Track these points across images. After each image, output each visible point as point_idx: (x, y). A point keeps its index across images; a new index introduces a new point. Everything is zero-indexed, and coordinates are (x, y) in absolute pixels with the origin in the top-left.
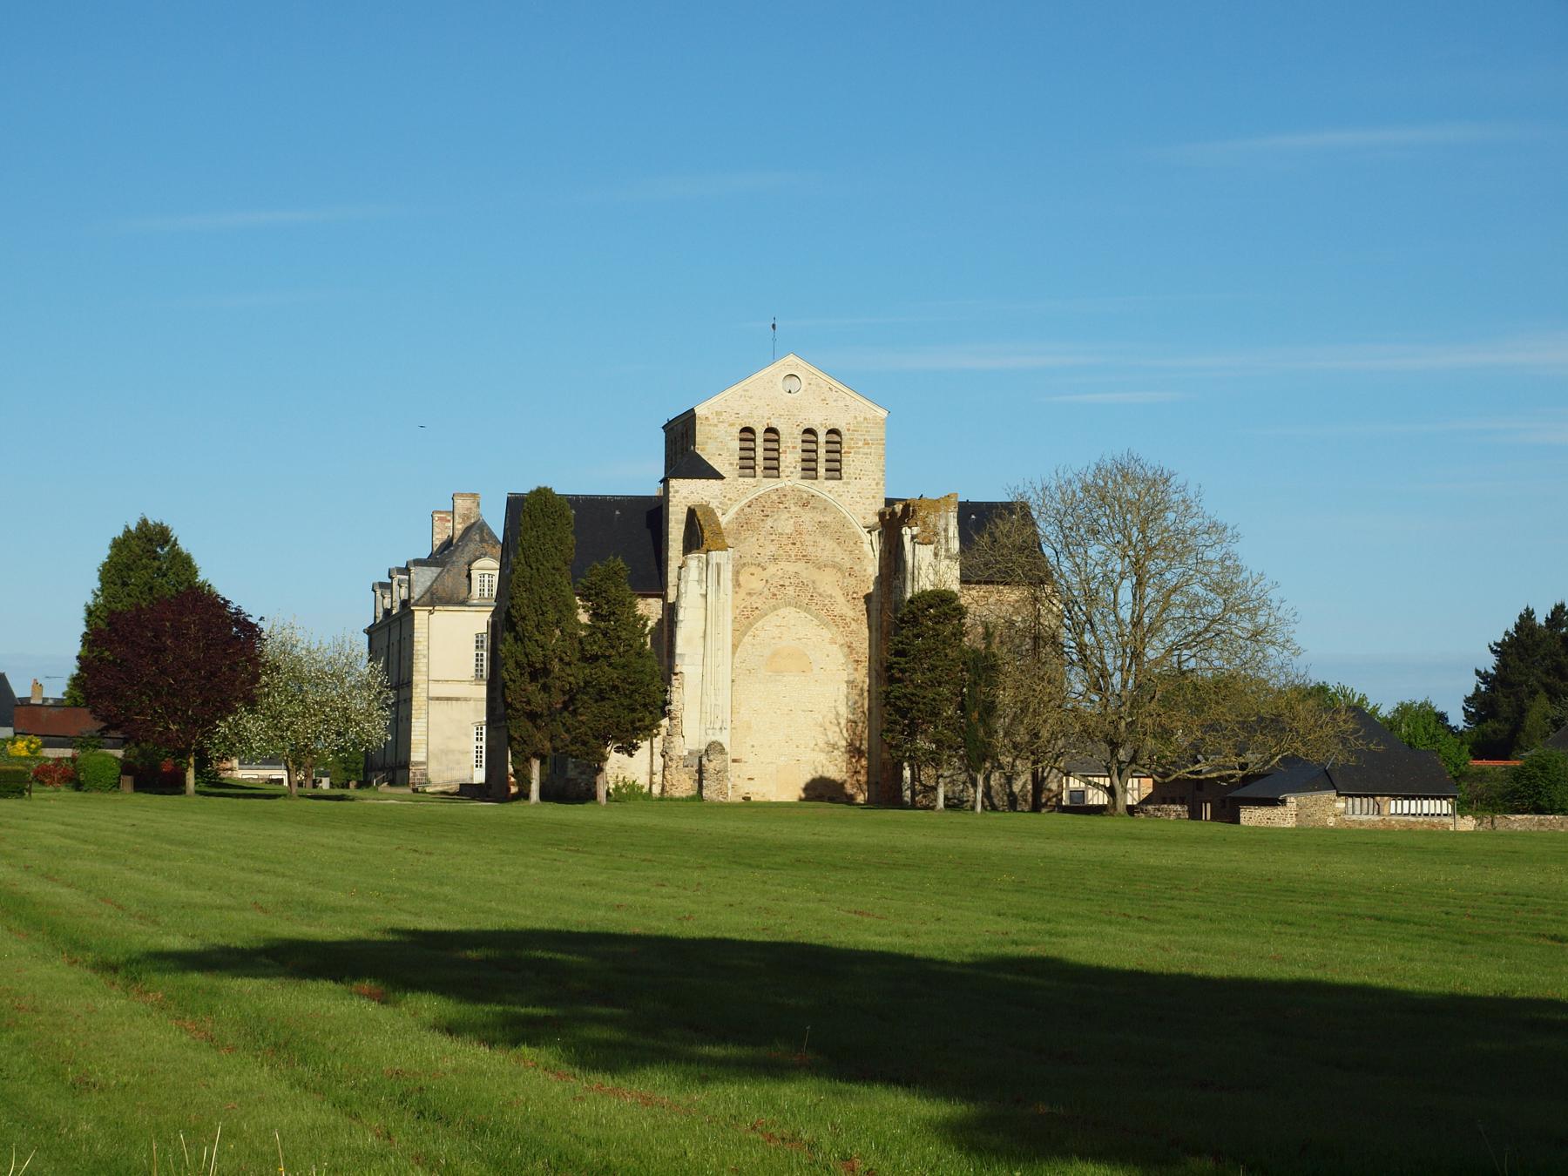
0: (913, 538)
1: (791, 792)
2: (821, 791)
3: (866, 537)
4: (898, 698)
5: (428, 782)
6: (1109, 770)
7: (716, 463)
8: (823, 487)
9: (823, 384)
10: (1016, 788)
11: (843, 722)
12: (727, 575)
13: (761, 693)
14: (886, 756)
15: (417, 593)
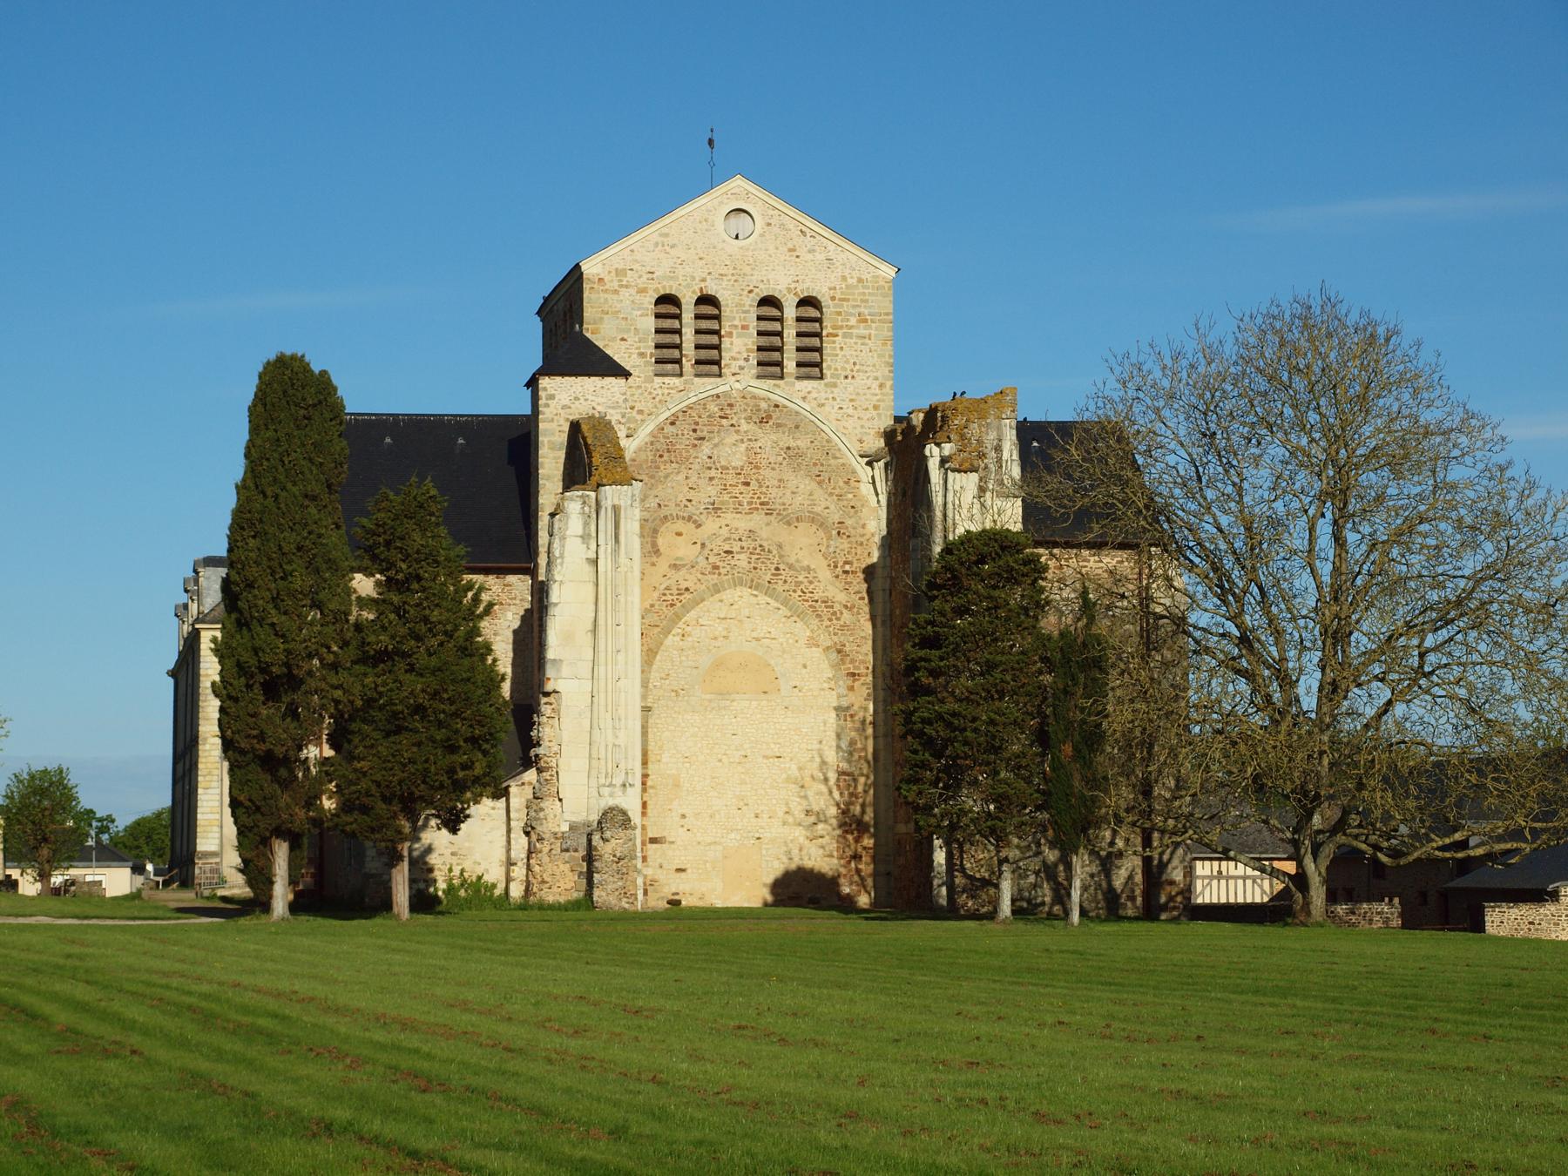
0: (943, 461)
1: (752, 893)
2: (799, 890)
3: (864, 473)
4: (928, 722)
6: (1296, 844)
8: (794, 392)
9: (791, 225)
10: (1118, 883)
11: (832, 776)
12: (631, 526)
13: (692, 721)
14: (902, 828)
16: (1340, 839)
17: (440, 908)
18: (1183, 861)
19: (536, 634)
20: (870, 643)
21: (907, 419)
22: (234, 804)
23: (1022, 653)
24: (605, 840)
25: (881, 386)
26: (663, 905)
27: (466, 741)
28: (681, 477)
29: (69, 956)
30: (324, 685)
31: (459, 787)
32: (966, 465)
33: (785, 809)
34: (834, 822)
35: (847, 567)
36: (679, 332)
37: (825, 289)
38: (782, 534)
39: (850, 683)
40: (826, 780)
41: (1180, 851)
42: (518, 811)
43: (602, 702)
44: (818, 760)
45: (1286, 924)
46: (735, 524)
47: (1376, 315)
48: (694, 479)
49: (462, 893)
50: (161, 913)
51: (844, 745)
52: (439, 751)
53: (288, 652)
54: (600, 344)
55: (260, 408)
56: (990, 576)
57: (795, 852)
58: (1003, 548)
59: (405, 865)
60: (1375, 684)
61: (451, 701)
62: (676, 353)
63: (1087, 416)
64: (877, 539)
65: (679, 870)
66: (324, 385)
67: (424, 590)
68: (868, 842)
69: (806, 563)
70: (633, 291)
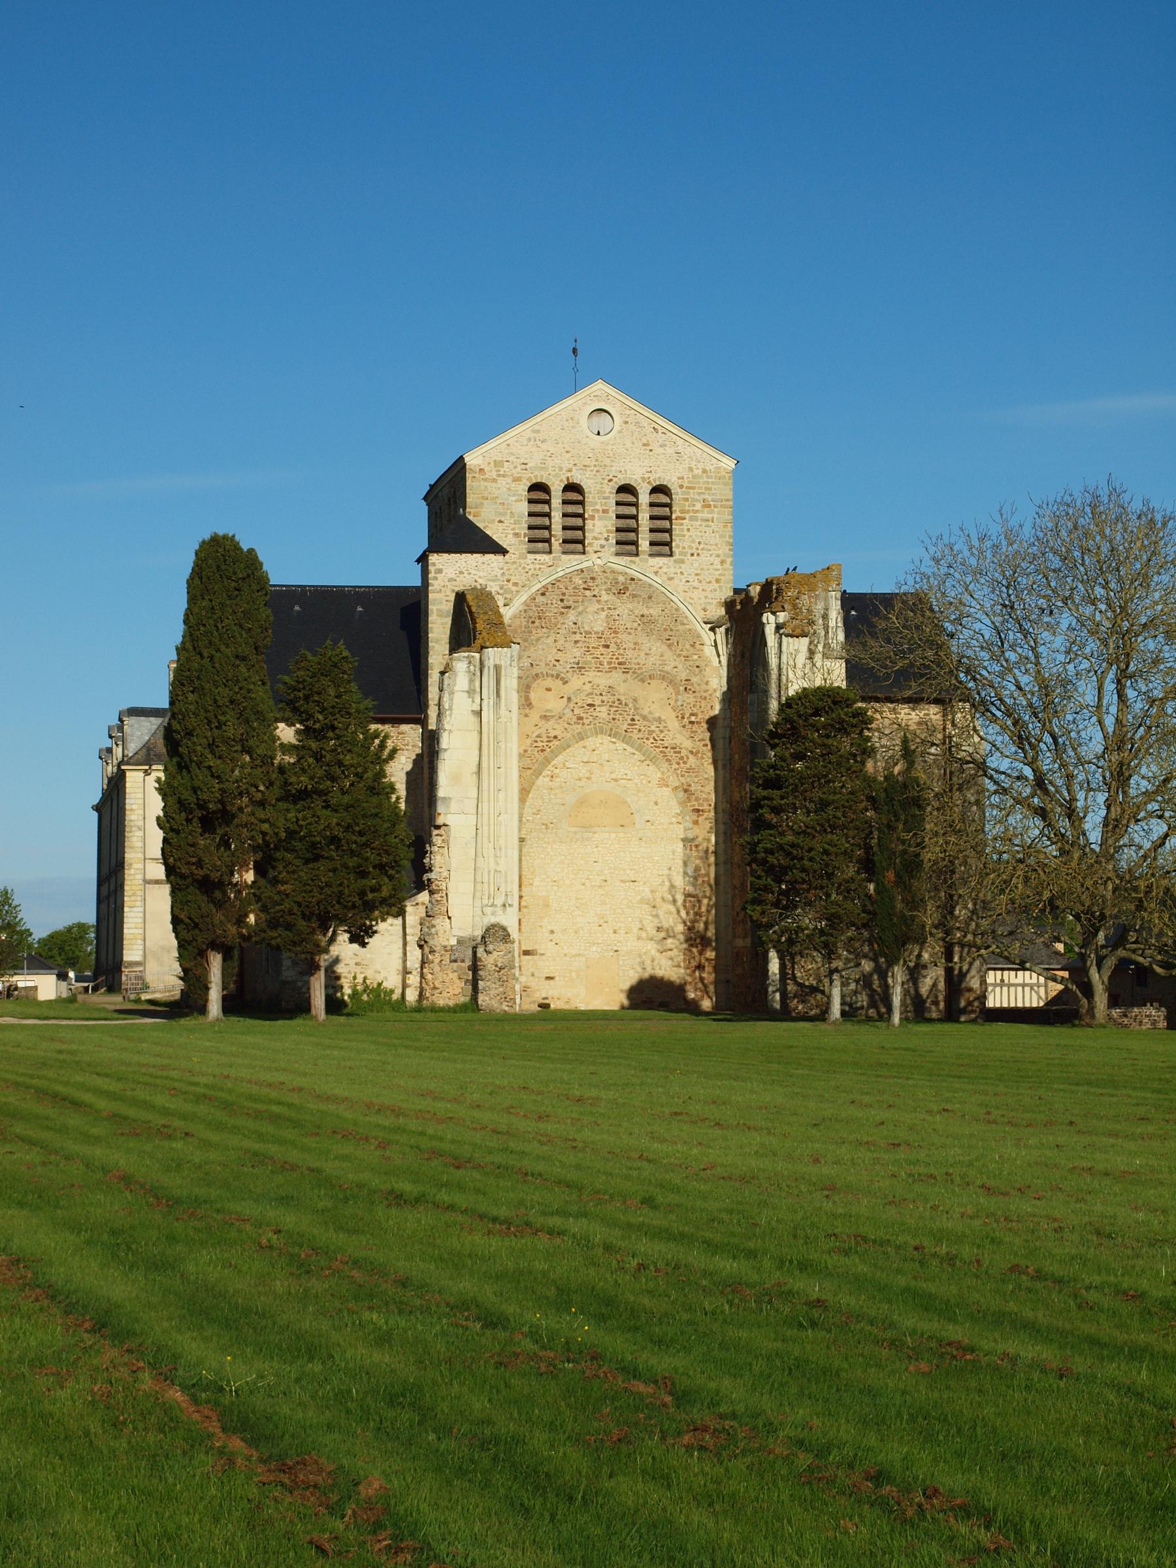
0: (778, 627)
1: (611, 998)
2: (650, 995)
3: (707, 637)
5: (146, 987)
7: (495, 533)
8: (647, 567)
9: (645, 422)
10: (924, 990)
11: (680, 898)
12: (510, 683)
13: (560, 853)
14: (739, 942)
15: (133, 747)
16: (1121, 953)
17: (345, 1011)
18: (979, 971)
19: (426, 775)
20: (712, 783)
21: (746, 591)
22: (176, 921)
23: (851, 793)
24: (488, 952)
25: (722, 562)
26: (535, 1008)
27: (374, 867)
28: (550, 640)
29: (60, 1052)
30: (253, 820)
31: (369, 908)
32: (798, 631)
33: (639, 926)
34: (682, 937)
35: (693, 719)
36: (548, 515)
37: (674, 479)
38: (637, 689)
39: (695, 817)
40: (675, 901)
41: (977, 963)
42: (413, 927)
43: (486, 834)
44: (667, 884)
45: (1074, 1026)
46: (597, 681)
47: (1155, 504)
48: (561, 642)
49: (365, 997)
50: (109, 1015)
51: (690, 871)
52: (352, 877)
53: (223, 791)
54: (480, 525)
55: (197, 581)
56: (824, 728)
57: (648, 962)
58: (835, 703)
59: (322, 974)
60: (1154, 821)
61: (361, 834)
62: (546, 534)
63: (904, 589)
64: (719, 694)
65: (548, 978)
66: (251, 561)
67: (338, 738)
68: (710, 954)
69: (657, 715)
70: (509, 480)
